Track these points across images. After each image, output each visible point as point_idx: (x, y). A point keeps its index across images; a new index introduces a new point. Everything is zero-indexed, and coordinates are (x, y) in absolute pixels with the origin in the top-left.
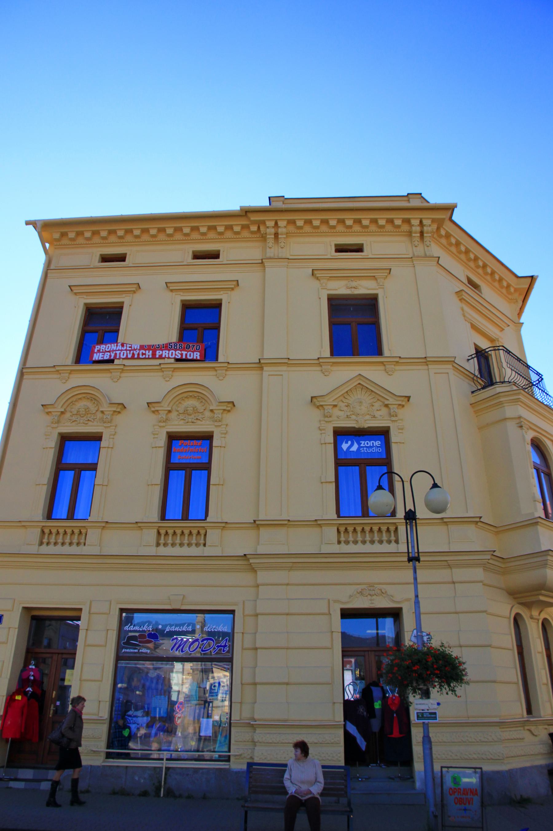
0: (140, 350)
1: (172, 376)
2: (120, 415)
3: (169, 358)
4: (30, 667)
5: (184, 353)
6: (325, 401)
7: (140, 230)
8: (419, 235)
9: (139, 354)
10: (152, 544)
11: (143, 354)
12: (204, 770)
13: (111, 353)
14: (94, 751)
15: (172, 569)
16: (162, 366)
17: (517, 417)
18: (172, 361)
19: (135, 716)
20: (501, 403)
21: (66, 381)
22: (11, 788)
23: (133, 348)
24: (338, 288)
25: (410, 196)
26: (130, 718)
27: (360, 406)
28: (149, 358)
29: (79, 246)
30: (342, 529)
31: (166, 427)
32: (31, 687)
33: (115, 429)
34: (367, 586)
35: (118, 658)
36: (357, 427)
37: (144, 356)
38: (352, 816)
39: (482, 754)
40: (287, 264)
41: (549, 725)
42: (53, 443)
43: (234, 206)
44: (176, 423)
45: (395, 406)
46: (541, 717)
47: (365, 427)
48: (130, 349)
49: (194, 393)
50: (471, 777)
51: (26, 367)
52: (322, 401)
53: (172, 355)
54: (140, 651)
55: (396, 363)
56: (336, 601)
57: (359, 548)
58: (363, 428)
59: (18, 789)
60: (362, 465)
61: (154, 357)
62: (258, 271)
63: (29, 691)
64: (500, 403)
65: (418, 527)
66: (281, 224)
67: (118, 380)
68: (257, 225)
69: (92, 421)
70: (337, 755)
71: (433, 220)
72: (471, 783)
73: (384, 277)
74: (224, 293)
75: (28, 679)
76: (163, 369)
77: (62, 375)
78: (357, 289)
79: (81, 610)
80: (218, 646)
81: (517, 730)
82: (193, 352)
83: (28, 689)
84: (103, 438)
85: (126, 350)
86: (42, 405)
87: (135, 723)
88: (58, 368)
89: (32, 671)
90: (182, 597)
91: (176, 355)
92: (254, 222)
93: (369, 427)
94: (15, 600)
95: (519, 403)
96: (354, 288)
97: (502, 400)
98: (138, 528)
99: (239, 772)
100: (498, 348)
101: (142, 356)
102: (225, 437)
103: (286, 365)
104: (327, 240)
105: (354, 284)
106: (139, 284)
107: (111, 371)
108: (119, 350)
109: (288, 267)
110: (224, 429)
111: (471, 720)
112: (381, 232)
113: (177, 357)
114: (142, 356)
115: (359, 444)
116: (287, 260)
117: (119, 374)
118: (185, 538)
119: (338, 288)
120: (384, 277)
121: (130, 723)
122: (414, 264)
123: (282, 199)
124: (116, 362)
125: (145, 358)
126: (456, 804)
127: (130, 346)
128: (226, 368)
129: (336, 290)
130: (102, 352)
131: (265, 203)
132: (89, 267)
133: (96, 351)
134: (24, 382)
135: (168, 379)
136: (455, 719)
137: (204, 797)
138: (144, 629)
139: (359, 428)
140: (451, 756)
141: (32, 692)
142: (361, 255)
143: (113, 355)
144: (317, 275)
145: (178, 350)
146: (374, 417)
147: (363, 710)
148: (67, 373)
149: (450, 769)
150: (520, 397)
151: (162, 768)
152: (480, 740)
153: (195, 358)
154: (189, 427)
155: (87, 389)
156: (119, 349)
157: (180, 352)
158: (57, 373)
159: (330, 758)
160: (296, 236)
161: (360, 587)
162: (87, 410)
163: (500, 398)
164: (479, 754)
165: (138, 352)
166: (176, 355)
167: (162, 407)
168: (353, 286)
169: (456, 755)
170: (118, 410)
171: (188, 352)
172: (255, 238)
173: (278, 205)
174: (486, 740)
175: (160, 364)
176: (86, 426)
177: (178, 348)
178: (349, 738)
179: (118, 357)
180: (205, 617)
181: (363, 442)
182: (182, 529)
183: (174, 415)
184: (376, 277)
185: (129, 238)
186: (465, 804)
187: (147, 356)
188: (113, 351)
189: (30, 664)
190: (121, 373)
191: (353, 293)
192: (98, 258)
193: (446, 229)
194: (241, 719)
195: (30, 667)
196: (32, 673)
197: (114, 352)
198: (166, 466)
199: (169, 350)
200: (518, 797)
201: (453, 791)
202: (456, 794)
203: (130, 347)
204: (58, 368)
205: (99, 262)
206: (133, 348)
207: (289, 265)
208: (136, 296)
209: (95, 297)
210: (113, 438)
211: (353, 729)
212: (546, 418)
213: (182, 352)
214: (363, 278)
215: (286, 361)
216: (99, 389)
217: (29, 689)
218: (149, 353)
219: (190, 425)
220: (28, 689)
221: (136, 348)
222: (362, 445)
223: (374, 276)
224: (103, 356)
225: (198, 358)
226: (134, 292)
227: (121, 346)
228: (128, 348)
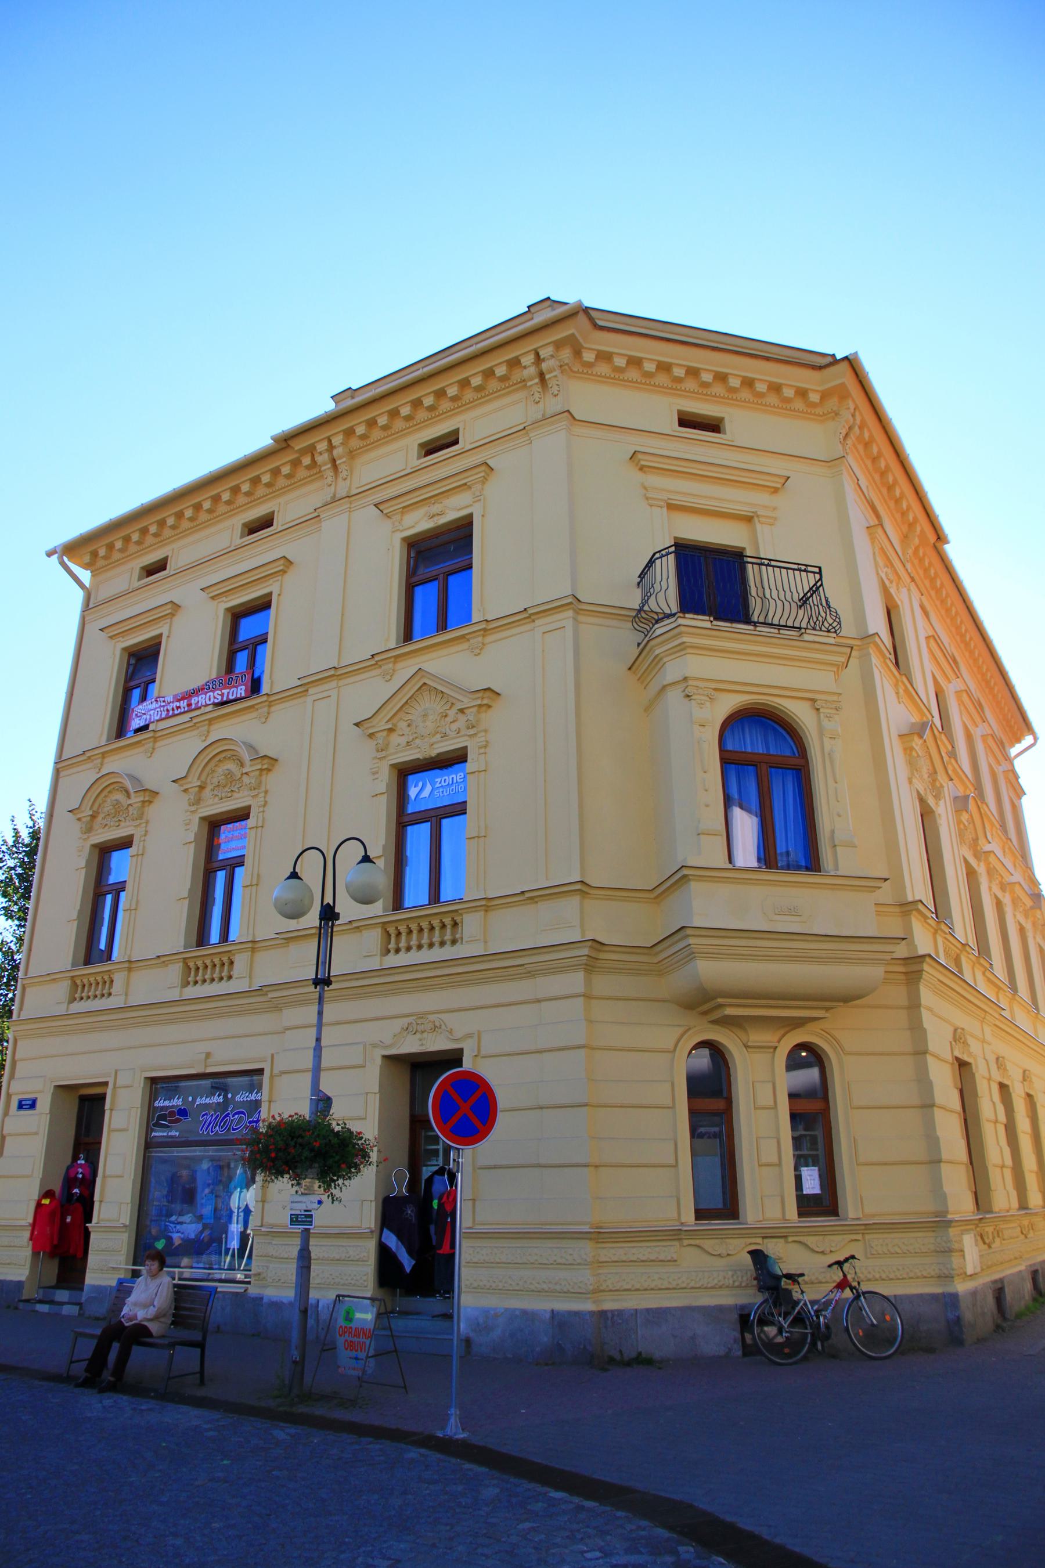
1: (394, 670)
2: (152, 805)
3: (207, 705)
4: (79, 1162)
5: (225, 691)
6: (373, 726)
7: (481, 374)
8: (537, 380)
10: (374, 953)
11: (178, 708)
14: (113, 1268)
15: (334, 997)
16: (195, 721)
17: (681, 679)
18: (210, 708)
19: (181, 1223)
21: (480, 650)
22: (37, 1311)
24: (416, 524)
26: (171, 1225)
27: (424, 721)
29: (116, 564)
30: (392, 930)
31: (199, 811)
32: (78, 1187)
33: (265, 797)
34: (415, 1018)
35: (149, 1145)
39: (556, 1284)
40: (348, 506)
41: (763, 1238)
42: (384, 781)
43: (262, 441)
44: (211, 802)
45: (474, 710)
46: (747, 1224)
47: (433, 755)
50: (366, 1312)
51: (473, 622)
52: (187, 783)
53: (210, 700)
54: (170, 1134)
55: (485, 632)
56: (374, 1046)
57: (425, 956)
58: (432, 758)
59: (43, 1313)
60: (434, 819)
61: (190, 708)
62: (524, 443)
63: (77, 1193)
64: (657, 660)
65: (334, 938)
66: (337, 440)
67: (391, 676)
68: (310, 454)
69: (237, 791)
70: (361, 1278)
71: (558, 345)
72: (365, 1320)
73: (481, 479)
74: (274, 582)
75: (76, 1177)
76: (379, 663)
77: (383, 668)
78: (443, 516)
79: (106, 1084)
80: (250, 1122)
81: (659, 1246)
83: (75, 1191)
84: (134, 843)
86: (357, 725)
87: (178, 1232)
88: (88, 754)
89: (81, 1167)
90: (203, 1056)
91: (215, 697)
92: (304, 451)
93: (439, 754)
95: (689, 650)
96: (438, 514)
97: (657, 652)
98: (529, 901)
99: (257, 1298)
100: (667, 550)
102: (485, 753)
103: (335, 678)
104: (228, 523)
105: (435, 508)
106: (286, 556)
107: (467, 637)
109: (352, 509)
110: (483, 739)
112: (482, 397)
113: (216, 701)
115: (433, 784)
116: (347, 499)
117: (480, 639)
118: (423, 937)
119: (416, 524)
120: (481, 479)
121: (173, 1232)
123: (350, 392)
124: (152, 727)
125: (181, 713)
126: (347, 1349)
128: (267, 703)
129: (413, 527)
131: (330, 406)
132: (230, 549)
134: (61, 780)
135: (478, 651)
136: (540, 1226)
138: (175, 1104)
139: (425, 759)
140: (511, 1285)
141: (80, 1194)
142: (453, 451)
145: (218, 690)
146: (445, 735)
147: (412, 1211)
148: (204, 725)
149: (346, 1298)
150: (685, 639)
151: (400, 1296)
152: (484, 1260)
153: (239, 696)
155: (217, 747)
157: (220, 692)
158: (89, 761)
159: (353, 1282)
160: (367, 450)
161: (406, 1021)
162: (229, 774)
163: (654, 652)
164: (550, 1282)
166: (215, 697)
167: (190, 782)
168: (435, 513)
169: (518, 1284)
170: (265, 766)
171: (230, 689)
172: (316, 474)
173: (349, 403)
174: (563, 1261)
175: (372, 656)
176: (230, 801)
177: (218, 686)
178: (384, 1254)
180: (252, 1080)
181: (439, 780)
182: (439, 917)
183: (207, 792)
184: (468, 484)
185: (445, 405)
186: (357, 1351)
187: (183, 710)
189: (79, 1159)
190: (484, 636)
191: (437, 525)
192: (414, 450)
193: (594, 347)
194: (262, 1226)
195: (79, 1162)
196: (80, 1170)
198: (205, 867)
200: (634, 1355)
201: (345, 1330)
202: (347, 1335)
204: (88, 754)
205: (419, 458)
207: (353, 505)
208: (287, 577)
210: (485, 753)
211: (392, 1240)
212: (779, 658)
213: (223, 691)
214: (450, 493)
215: (332, 672)
216: (232, 739)
217: (76, 1190)
218: (183, 704)
219: (226, 801)
220: (75, 1191)
222: (438, 785)
223: (465, 484)
225: (243, 695)
226: (284, 572)
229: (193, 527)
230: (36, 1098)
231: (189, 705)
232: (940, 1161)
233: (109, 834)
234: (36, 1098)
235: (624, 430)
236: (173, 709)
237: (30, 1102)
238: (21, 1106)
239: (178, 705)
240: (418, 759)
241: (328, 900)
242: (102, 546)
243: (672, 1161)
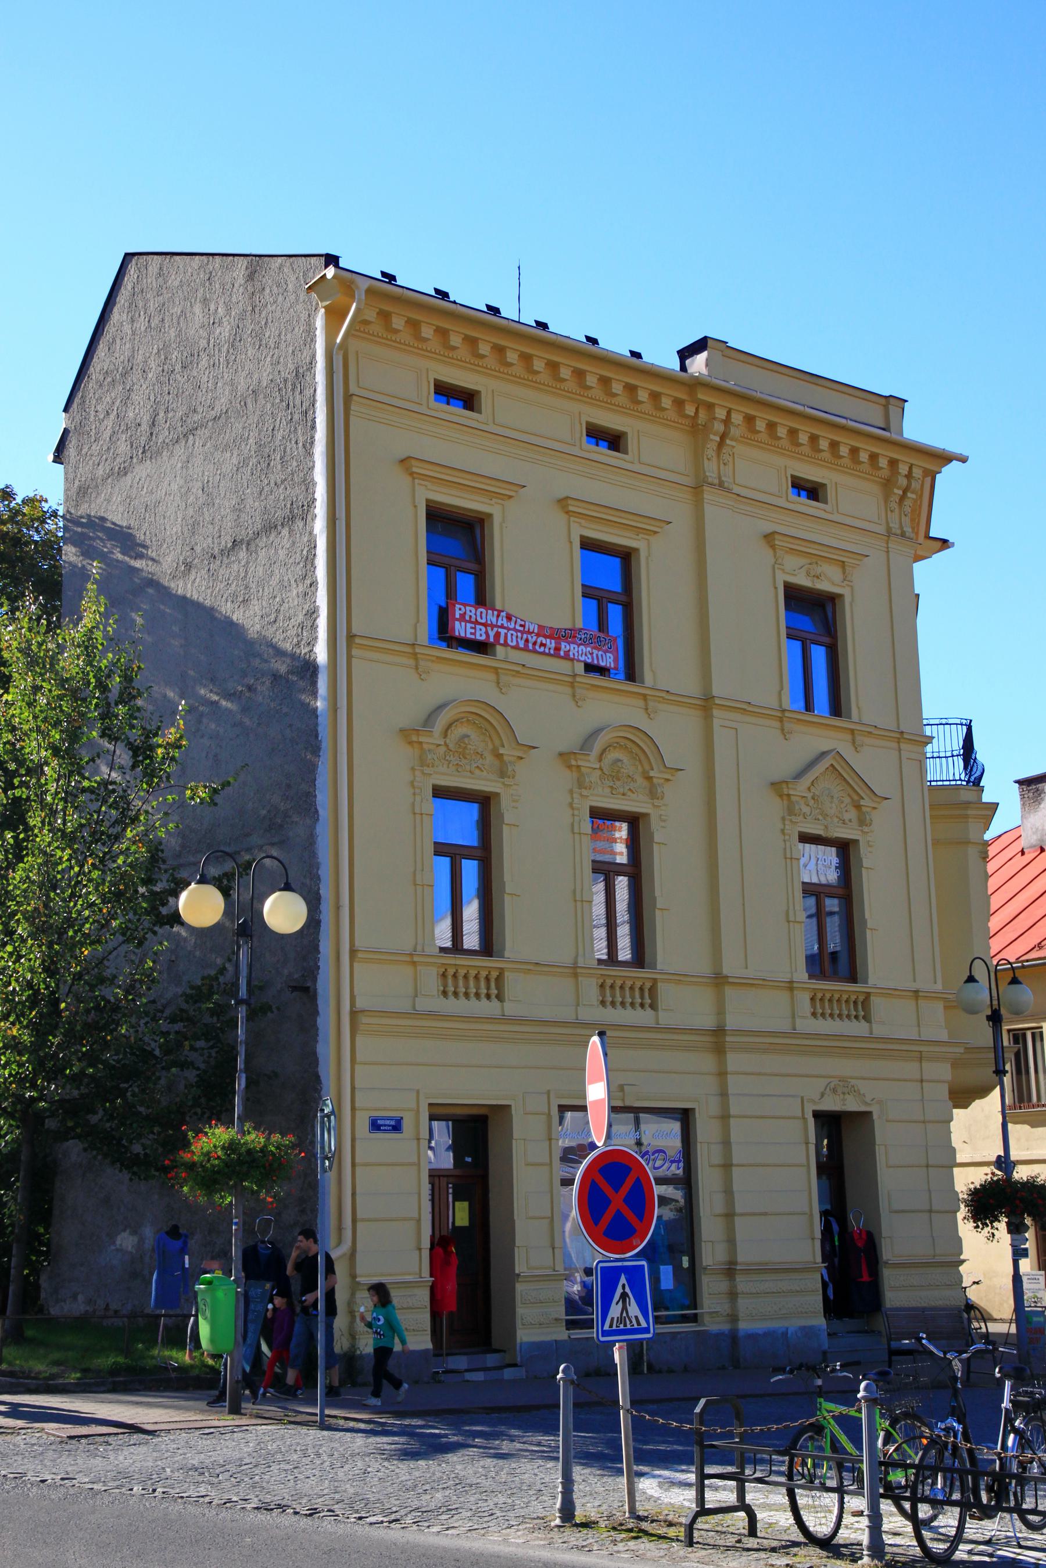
0: (538, 635)
9: (535, 644)
11: (542, 645)
12: (683, 1335)
13: (489, 629)
20: (966, 817)
22: (468, 1381)
23: (526, 629)
25: (891, 400)
28: (549, 654)
36: (824, 835)
37: (542, 649)
38: (469, 1159)
48: (521, 629)
49: (627, 742)
82: (579, 646)
85: (515, 629)
94: (418, 1092)
101: (540, 647)
108: (502, 627)
111: (938, 1259)
114: (540, 647)
122: (888, 548)
125: (543, 653)
127: (523, 623)
130: (470, 622)
133: (457, 616)
137: (686, 1369)
143: (492, 634)
144: (415, 470)
154: (616, 801)
156: (502, 624)
165: (535, 638)
167: (589, 761)
172: (682, 424)
179: (502, 641)
188: (493, 626)
194: (714, 1264)
197: (495, 629)
199: (579, 646)
203: (521, 625)
206: (526, 629)
209: (612, 531)
218: (551, 644)
221: (531, 630)
224: (473, 631)
227: (505, 619)
228: (518, 627)
229: (524, 379)
230: (402, 1118)
231: (557, 649)
232: (731, 1165)
233: (469, 781)
234: (402, 1118)
235: (853, 529)
236: (535, 644)
237: (393, 1123)
238: (375, 1126)
239: (544, 642)
240: (820, 835)
241: (995, 1006)
242: (404, 316)
243: (415, 1159)
